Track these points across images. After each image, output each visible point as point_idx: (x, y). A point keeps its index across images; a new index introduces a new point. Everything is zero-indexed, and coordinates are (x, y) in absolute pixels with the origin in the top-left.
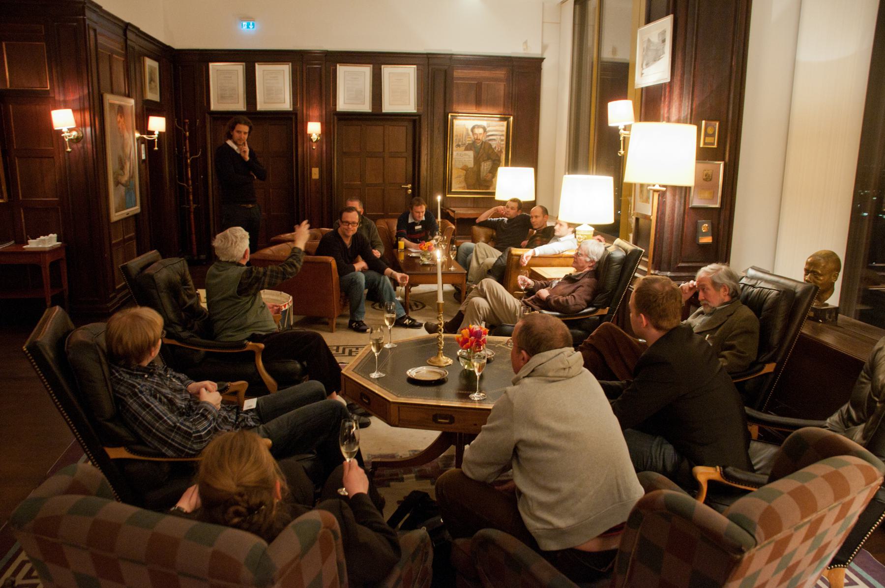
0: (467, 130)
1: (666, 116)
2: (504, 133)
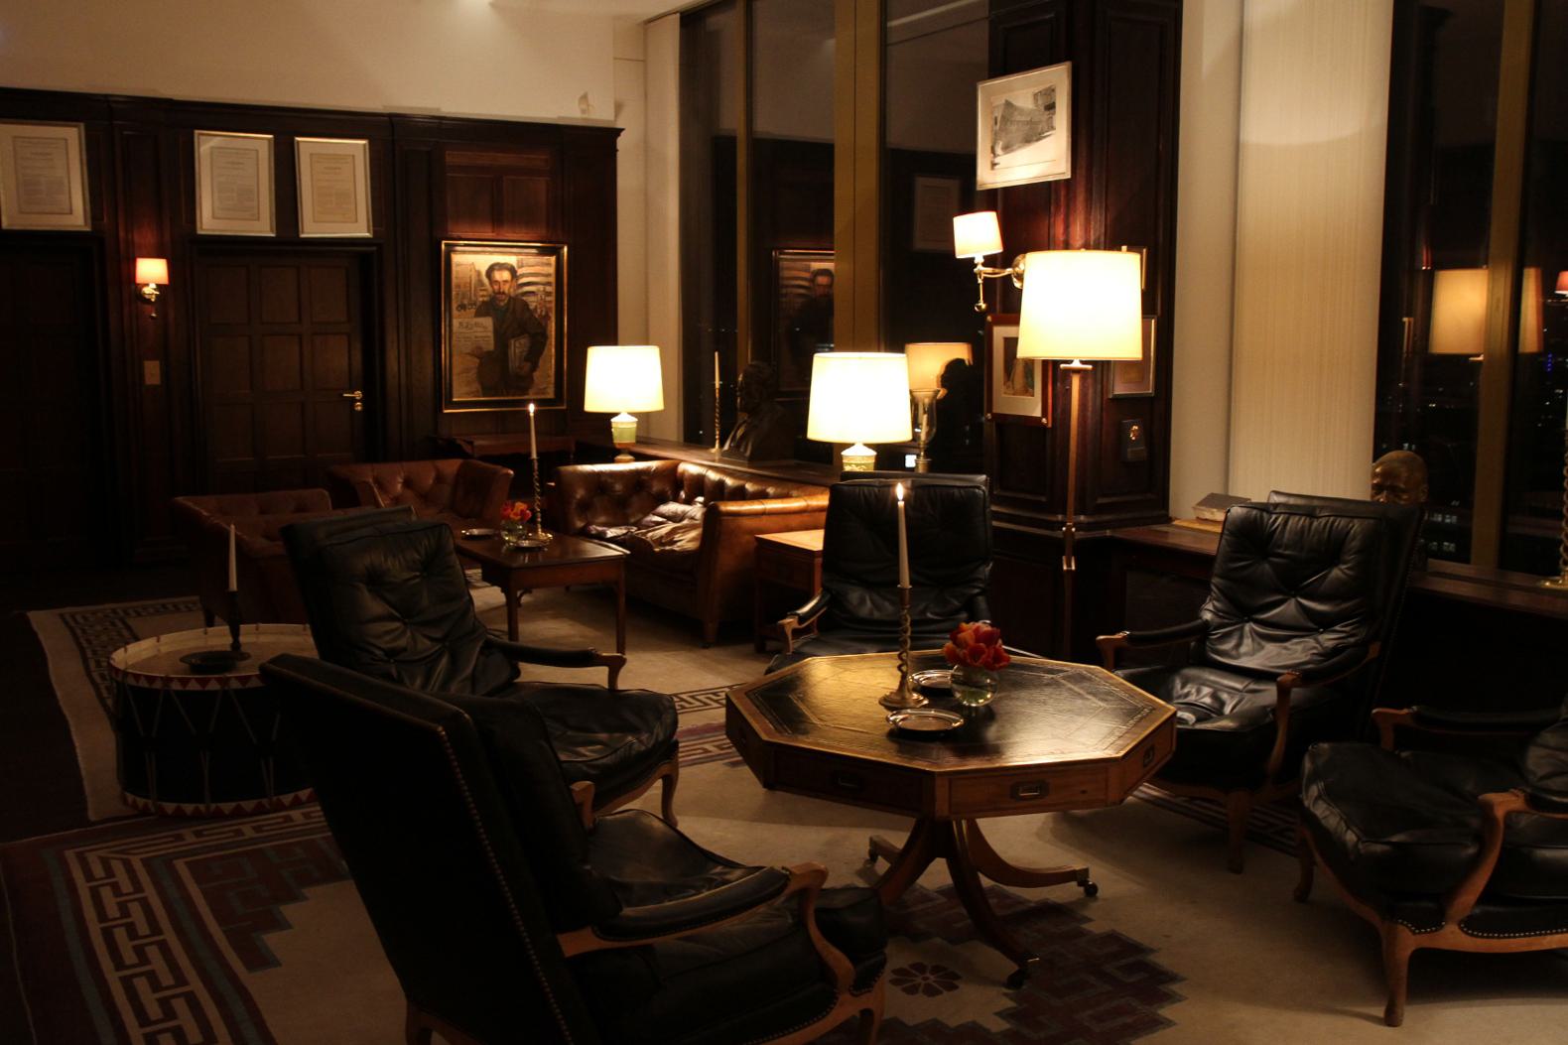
0: (479, 273)
1: (1061, 238)
2: (552, 279)
